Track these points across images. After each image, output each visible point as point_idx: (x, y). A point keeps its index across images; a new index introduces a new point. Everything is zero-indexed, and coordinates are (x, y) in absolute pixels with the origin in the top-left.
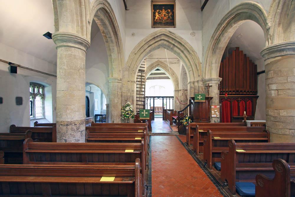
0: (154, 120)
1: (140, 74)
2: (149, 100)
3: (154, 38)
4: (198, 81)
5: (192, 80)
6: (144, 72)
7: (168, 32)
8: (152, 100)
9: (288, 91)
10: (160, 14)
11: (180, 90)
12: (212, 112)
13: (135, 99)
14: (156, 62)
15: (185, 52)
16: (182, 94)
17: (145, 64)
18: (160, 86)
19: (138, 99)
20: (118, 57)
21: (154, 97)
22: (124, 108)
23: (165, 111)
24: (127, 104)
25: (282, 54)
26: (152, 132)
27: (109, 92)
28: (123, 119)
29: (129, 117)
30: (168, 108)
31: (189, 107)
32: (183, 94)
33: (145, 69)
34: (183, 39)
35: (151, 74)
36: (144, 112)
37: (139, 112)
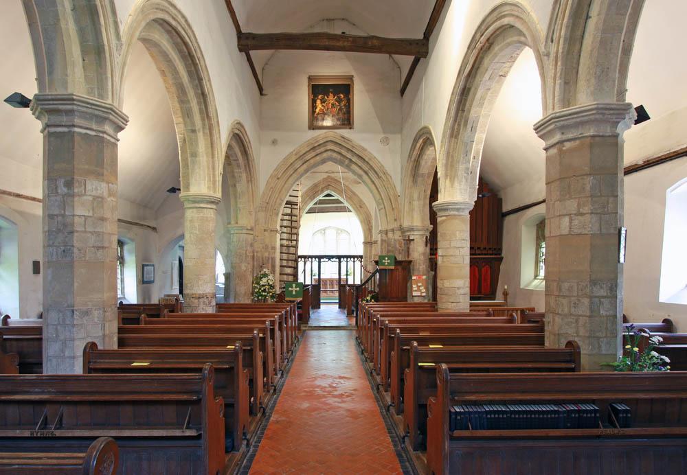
0: (319, 308)
1: (289, 211)
2: (308, 264)
3: (314, 148)
4: (393, 230)
5: (384, 227)
6: (295, 207)
7: (340, 138)
9: (452, 258)
10: (324, 102)
12: (414, 286)
13: (278, 263)
14: (325, 179)
15: (371, 173)
17: (299, 188)
18: (338, 229)
19: (285, 263)
20: (248, 187)
21: (320, 257)
22: (257, 279)
23: (342, 287)
24: (262, 272)
25: (447, 213)
26: (309, 325)
27: (229, 250)
28: (256, 299)
29: (266, 296)
31: (373, 278)
33: (299, 200)
34: (366, 150)
35: (321, 202)
36: (292, 288)
37: (284, 288)
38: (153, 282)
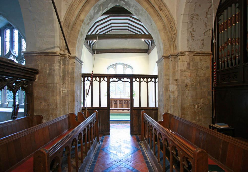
2: (144, 84)
8: (104, 84)
11: (182, 54)
16: (186, 64)
21: (109, 76)
30: (144, 105)
32: (189, 64)
38: (163, 56)
